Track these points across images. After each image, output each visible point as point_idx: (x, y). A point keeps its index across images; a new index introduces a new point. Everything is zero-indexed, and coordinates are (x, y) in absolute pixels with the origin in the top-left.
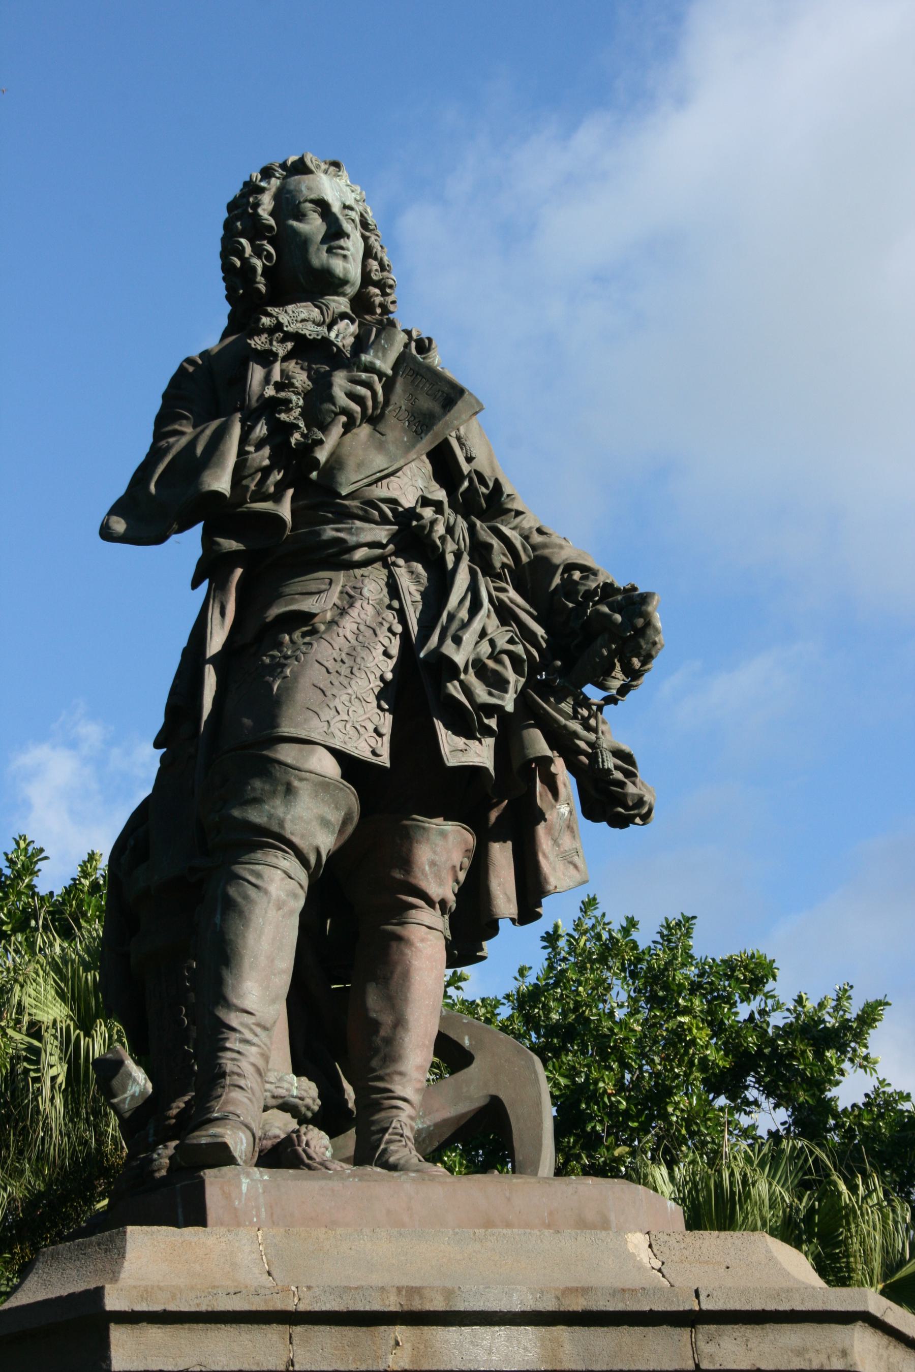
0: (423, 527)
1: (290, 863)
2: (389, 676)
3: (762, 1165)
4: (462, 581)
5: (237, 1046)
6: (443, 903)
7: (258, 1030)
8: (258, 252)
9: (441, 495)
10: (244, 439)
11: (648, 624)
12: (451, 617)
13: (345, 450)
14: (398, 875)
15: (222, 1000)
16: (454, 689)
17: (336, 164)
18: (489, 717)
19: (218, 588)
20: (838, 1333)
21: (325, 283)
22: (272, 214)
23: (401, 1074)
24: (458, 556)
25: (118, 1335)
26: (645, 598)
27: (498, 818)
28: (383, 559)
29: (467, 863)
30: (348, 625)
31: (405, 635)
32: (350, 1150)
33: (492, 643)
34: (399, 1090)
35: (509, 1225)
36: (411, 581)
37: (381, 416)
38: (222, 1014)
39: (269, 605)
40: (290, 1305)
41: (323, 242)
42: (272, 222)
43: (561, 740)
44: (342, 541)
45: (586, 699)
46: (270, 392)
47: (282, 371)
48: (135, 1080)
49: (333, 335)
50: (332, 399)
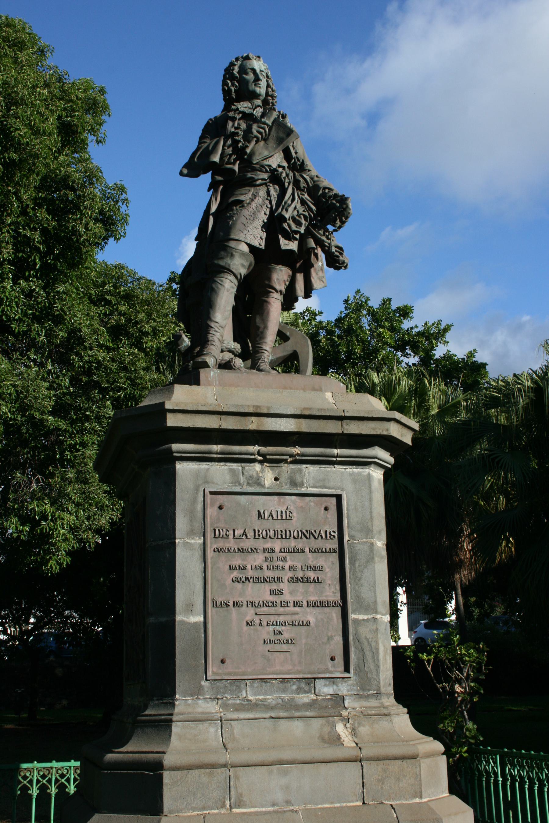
0: (278, 174)
1: (232, 278)
2: (266, 221)
3: (405, 374)
4: (290, 191)
5: (213, 332)
6: (281, 292)
7: (220, 328)
8: (233, 85)
9: (285, 164)
10: (224, 145)
11: (347, 206)
12: (285, 203)
13: (256, 149)
14: (267, 282)
15: (209, 318)
16: (285, 225)
17: (259, 57)
18: (296, 234)
19: (215, 192)
20: (386, 424)
21: (254, 95)
22: (238, 73)
23: (265, 343)
24: (289, 184)
25: (169, 416)
26: (347, 199)
27: (299, 266)
28: (266, 184)
29: (289, 279)
30: (254, 205)
31: (271, 208)
32: (249, 365)
33: (298, 211)
34: (264, 347)
35: (291, 389)
36: (274, 191)
37: (268, 138)
38: (209, 323)
39: (230, 198)
40: (221, 409)
41: (254, 82)
42: (238, 75)
43: (320, 243)
44: (253, 178)
45: (328, 229)
46: (233, 130)
47: (238, 124)
48: (185, 341)
49: (255, 112)
50: (252, 133)
